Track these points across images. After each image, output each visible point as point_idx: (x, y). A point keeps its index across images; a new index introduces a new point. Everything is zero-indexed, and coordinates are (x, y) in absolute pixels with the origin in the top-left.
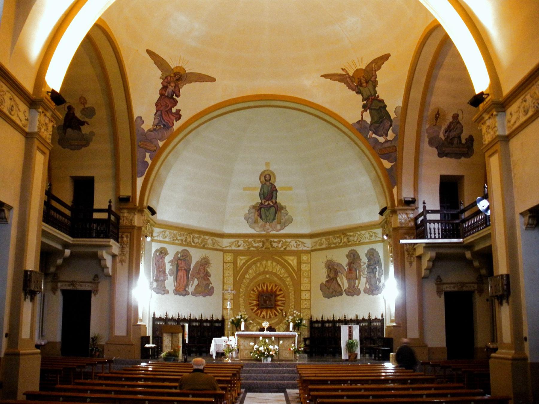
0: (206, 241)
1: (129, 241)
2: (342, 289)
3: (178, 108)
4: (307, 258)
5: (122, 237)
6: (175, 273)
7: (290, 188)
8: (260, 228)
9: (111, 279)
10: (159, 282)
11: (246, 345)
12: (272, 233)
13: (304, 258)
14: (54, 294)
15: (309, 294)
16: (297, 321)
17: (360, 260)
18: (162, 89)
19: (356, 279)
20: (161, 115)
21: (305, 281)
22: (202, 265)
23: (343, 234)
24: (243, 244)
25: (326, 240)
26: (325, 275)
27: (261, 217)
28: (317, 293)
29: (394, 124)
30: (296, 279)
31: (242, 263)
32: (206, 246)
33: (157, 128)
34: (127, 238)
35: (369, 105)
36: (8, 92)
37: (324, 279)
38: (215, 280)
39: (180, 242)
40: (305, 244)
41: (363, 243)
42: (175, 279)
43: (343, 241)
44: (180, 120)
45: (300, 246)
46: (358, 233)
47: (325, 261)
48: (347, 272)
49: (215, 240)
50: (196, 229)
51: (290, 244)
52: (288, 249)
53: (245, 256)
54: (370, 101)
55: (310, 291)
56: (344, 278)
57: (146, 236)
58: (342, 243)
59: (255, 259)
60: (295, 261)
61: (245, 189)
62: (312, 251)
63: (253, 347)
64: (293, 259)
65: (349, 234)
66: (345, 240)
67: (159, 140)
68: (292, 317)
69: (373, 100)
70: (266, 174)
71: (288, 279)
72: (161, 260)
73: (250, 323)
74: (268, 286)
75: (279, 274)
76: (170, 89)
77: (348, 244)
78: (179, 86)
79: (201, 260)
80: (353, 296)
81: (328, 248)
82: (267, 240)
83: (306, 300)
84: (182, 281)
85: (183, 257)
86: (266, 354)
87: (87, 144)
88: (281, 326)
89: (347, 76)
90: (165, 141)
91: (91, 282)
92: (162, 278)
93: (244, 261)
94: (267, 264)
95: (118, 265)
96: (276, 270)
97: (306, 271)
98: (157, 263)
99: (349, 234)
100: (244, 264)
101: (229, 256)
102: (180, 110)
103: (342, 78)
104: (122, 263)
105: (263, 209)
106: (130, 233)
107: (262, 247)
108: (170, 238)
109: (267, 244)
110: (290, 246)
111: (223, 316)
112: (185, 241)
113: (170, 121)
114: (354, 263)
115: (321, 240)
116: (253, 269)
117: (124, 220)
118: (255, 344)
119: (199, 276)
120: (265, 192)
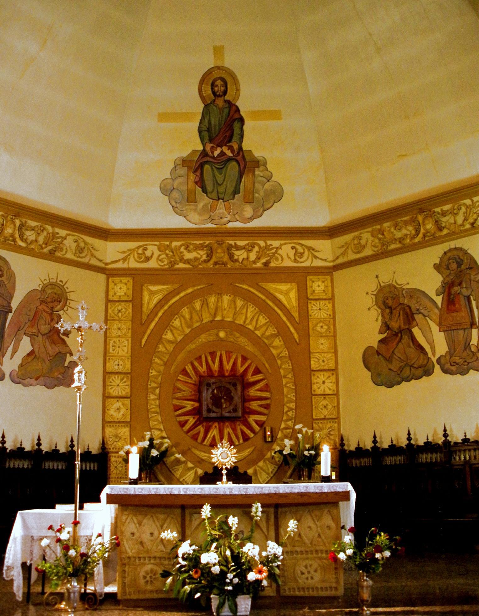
2: (429, 359)
4: (322, 287)
8: (200, 214)
11: (146, 537)
12: (230, 225)
13: (315, 286)
15: (333, 379)
16: (306, 453)
22: (43, 302)
23: (421, 211)
24: (157, 253)
27: (205, 191)
31: (155, 300)
32: (58, 254)
40: (316, 251)
46: (468, 202)
47: (373, 287)
48: (440, 310)
49: (84, 241)
50: (32, 205)
51: (280, 251)
52: (272, 265)
55: (334, 371)
56: (435, 327)
58: (421, 235)
59: (189, 291)
60: (293, 295)
61: (163, 117)
63: (176, 546)
64: (288, 291)
65: (438, 210)
66: (430, 226)
68: (292, 442)
71: (277, 342)
73: (178, 461)
74: (225, 362)
75: (252, 328)
79: (43, 290)
80: (464, 372)
82: (220, 244)
83: (324, 395)
86: (231, 583)
88: (261, 468)
93: (159, 297)
94: (220, 304)
96: (244, 317)
97: (320, 320)
100: (160, 304)
101: (120, 285)
105: (207, 167)
107: (205, 261)
111: (103, 443)
114: (460, 284)
115: (360, 238)
116: (184, 317)
118: (183, 539)
119: (34, 330)
120: (213, 123)
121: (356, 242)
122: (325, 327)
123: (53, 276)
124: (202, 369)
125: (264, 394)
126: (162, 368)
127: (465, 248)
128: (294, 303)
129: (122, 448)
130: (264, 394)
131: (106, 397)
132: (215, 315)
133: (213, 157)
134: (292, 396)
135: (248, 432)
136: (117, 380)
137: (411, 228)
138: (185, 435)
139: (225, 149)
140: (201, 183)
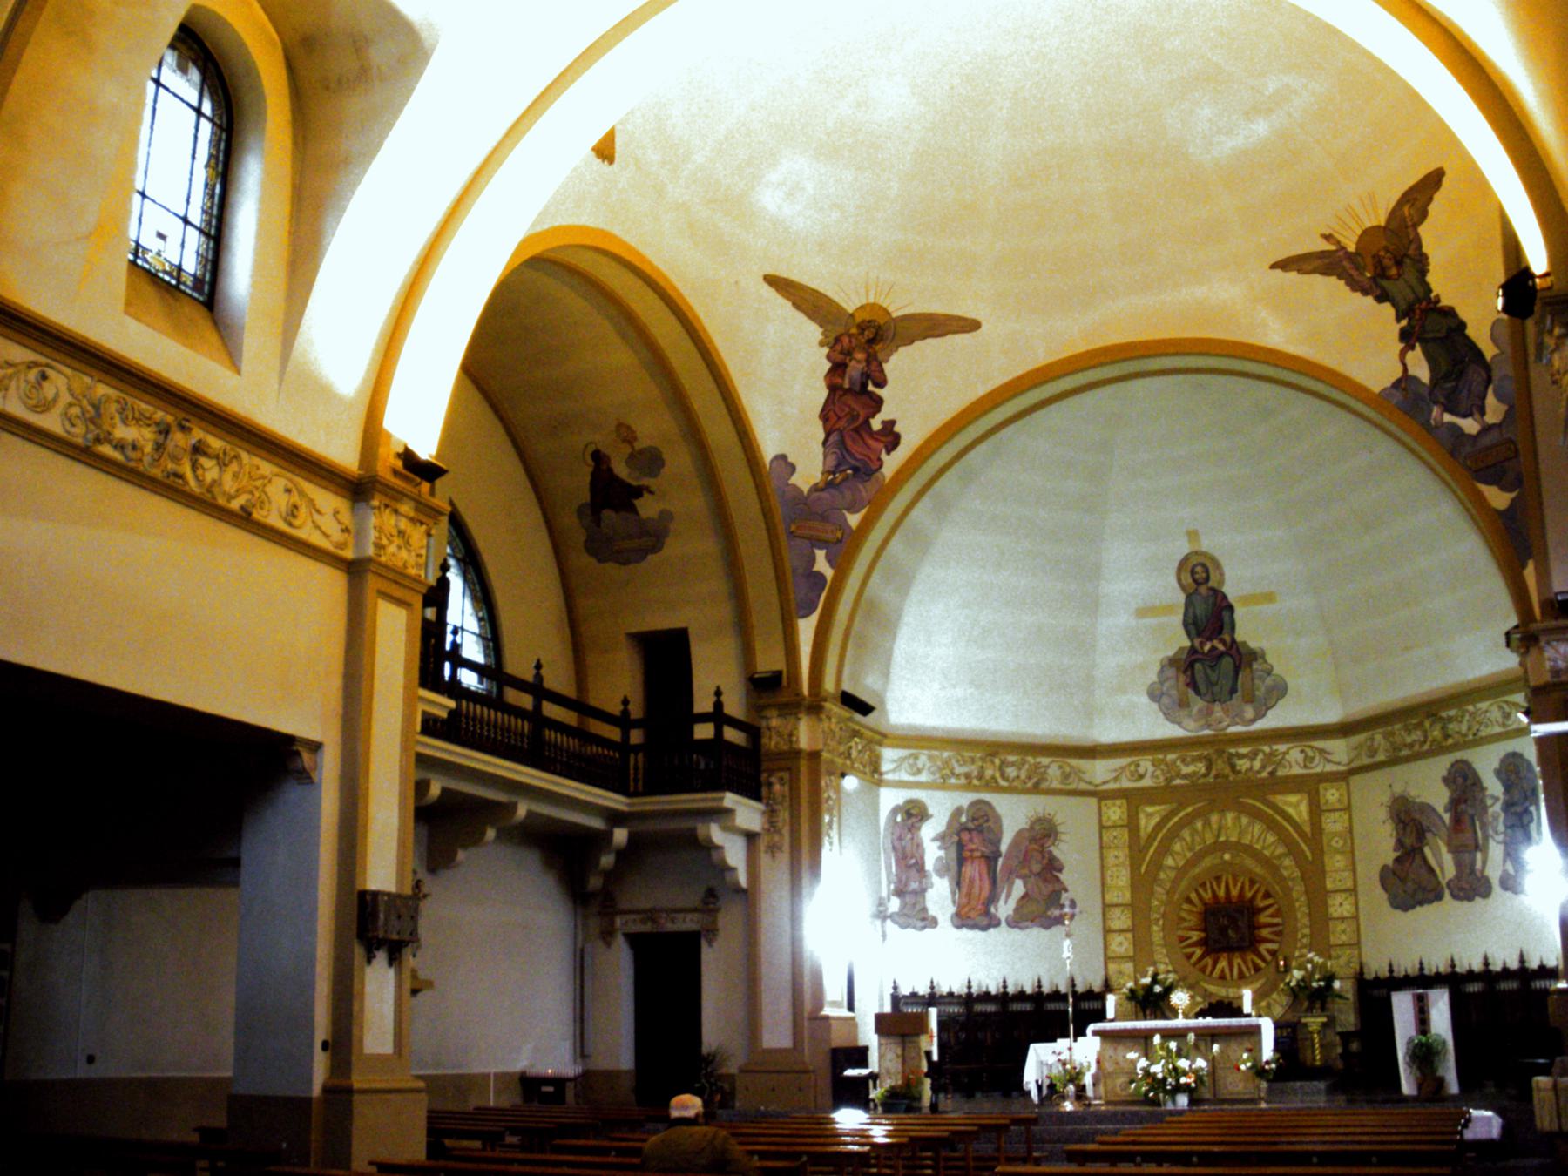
0: (1043, 770)
1: (787, 794)
2: (1439, 883)
3: (887, 418)
4: (1337, 795)
5: (770, 785)
6: (954, 865)
7: (1269, 597)
8: (1195, 721)
9: (748, 897)
10: (908, 899)
11: (1120, 1059)
14: (608, 944)
17: (1483, 789)
18: (831, 372)
19: (1477, 847)
20: (842, 443)
21: (1335, 863)
23: (1429, 715)
24: (1151, 769)
25: (1384, 737)
26: (1390, 842)
27: (1198, 693)
28: (1374, 897)
29: (1496, 374)
30: (1310, 858)
31: (1291, 811)
32: (1044, 786)
33: (835, 478)
34: (782, 785)
35: (1417, 329)
36: (277, 475)
37: (1388, 855)
38: (1078, 877)
39: (963, 781)
40: (1329, 754)
41: (1486, 737)
42: (954, 884)
43: (1430, 738)
44: (899, 448)
45: (1316, 761)
46: (1471, 708)
47: (1385, 798)
48: (1448, 829)
49: (1069, 765)
51: (1287, 757)
52: (1280, 773)
53: (1160, 804)
54: (1417, 317)
55: (1353, 891)
56: (1444, 849)
57: (843, 775)
58: (1428, 743)
59: (1189, 809)
60: (1304, 807)
62: (1353, 772)
65: (1444, 714)
66: (1437, 733)
67: (848, 510)
68: (1302, 973)
69: (1425, 312)
70: (1195, 562)
71: (1288, 862)
72: (909, 836)
76: (855, 368)
77: (1444, 744)
78: (880, 356)
79: (1032, 828)
80: (1470, 899)
81: (1393, 761)
82: (1220, 752)
83: (1343, 919)
84: (976, 890)
85: (976, 823)
87: (656, 548)
88: (1275, 1000)
89: (1341, 253)
90: (864, 512)
91: (695, 910)
92: (914, 885)
95: (764, 859)
96: (1249, 837)
97: (1335, 834)
98: (897, 844)
99: (1444, 714)
100: (1159, 826)
101: (1113, 809)
102: (893, 423)
103: (1329, 262)
104: (772, 852)
105: (1198, 666)
106: (789, 769)
107: (1205, 776)
108: (933, 773)
109: (1220, 765)
110: (1287, 764)
112: (980, 777)
113: (872, 457)
114: (1466, 801)
115: (1372, 739)
116: (1184, 840)
117: (770, 738)
119: (1026, 871)
121: (1369, 743)
122: (1341, 843)
123: (1040, 810)
124: (1208, 896)
125: (1276, 920)
126: (1164, 897)
127: (1470, 760)
128: (1305, 815)
129: (1124, 985)
130: (1276, 920)
131: (1107, 931)
132: (1218, 836)
133: (1203, 653)
134: (1306, 921)
135: (1258, 961)
136: (1117, 912)
137: (1419, 733)
138: (1191, 968)
139: (1216, 643)
140: (1193, 684)
